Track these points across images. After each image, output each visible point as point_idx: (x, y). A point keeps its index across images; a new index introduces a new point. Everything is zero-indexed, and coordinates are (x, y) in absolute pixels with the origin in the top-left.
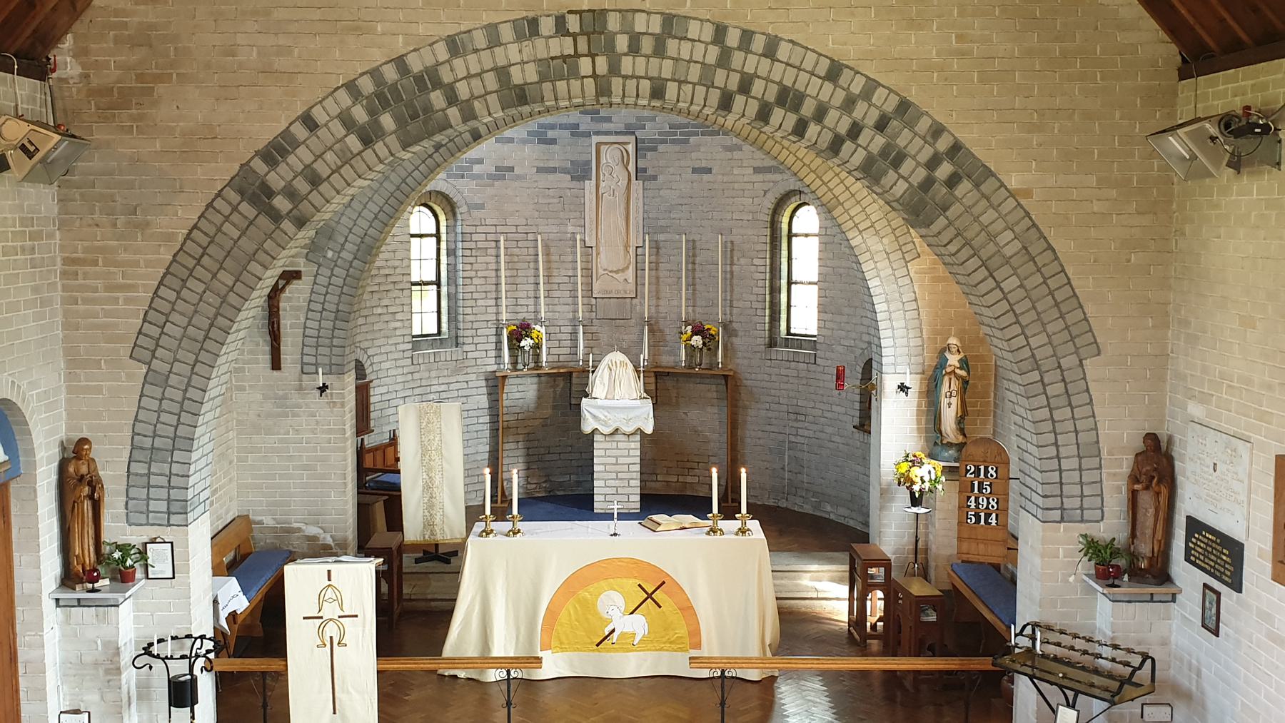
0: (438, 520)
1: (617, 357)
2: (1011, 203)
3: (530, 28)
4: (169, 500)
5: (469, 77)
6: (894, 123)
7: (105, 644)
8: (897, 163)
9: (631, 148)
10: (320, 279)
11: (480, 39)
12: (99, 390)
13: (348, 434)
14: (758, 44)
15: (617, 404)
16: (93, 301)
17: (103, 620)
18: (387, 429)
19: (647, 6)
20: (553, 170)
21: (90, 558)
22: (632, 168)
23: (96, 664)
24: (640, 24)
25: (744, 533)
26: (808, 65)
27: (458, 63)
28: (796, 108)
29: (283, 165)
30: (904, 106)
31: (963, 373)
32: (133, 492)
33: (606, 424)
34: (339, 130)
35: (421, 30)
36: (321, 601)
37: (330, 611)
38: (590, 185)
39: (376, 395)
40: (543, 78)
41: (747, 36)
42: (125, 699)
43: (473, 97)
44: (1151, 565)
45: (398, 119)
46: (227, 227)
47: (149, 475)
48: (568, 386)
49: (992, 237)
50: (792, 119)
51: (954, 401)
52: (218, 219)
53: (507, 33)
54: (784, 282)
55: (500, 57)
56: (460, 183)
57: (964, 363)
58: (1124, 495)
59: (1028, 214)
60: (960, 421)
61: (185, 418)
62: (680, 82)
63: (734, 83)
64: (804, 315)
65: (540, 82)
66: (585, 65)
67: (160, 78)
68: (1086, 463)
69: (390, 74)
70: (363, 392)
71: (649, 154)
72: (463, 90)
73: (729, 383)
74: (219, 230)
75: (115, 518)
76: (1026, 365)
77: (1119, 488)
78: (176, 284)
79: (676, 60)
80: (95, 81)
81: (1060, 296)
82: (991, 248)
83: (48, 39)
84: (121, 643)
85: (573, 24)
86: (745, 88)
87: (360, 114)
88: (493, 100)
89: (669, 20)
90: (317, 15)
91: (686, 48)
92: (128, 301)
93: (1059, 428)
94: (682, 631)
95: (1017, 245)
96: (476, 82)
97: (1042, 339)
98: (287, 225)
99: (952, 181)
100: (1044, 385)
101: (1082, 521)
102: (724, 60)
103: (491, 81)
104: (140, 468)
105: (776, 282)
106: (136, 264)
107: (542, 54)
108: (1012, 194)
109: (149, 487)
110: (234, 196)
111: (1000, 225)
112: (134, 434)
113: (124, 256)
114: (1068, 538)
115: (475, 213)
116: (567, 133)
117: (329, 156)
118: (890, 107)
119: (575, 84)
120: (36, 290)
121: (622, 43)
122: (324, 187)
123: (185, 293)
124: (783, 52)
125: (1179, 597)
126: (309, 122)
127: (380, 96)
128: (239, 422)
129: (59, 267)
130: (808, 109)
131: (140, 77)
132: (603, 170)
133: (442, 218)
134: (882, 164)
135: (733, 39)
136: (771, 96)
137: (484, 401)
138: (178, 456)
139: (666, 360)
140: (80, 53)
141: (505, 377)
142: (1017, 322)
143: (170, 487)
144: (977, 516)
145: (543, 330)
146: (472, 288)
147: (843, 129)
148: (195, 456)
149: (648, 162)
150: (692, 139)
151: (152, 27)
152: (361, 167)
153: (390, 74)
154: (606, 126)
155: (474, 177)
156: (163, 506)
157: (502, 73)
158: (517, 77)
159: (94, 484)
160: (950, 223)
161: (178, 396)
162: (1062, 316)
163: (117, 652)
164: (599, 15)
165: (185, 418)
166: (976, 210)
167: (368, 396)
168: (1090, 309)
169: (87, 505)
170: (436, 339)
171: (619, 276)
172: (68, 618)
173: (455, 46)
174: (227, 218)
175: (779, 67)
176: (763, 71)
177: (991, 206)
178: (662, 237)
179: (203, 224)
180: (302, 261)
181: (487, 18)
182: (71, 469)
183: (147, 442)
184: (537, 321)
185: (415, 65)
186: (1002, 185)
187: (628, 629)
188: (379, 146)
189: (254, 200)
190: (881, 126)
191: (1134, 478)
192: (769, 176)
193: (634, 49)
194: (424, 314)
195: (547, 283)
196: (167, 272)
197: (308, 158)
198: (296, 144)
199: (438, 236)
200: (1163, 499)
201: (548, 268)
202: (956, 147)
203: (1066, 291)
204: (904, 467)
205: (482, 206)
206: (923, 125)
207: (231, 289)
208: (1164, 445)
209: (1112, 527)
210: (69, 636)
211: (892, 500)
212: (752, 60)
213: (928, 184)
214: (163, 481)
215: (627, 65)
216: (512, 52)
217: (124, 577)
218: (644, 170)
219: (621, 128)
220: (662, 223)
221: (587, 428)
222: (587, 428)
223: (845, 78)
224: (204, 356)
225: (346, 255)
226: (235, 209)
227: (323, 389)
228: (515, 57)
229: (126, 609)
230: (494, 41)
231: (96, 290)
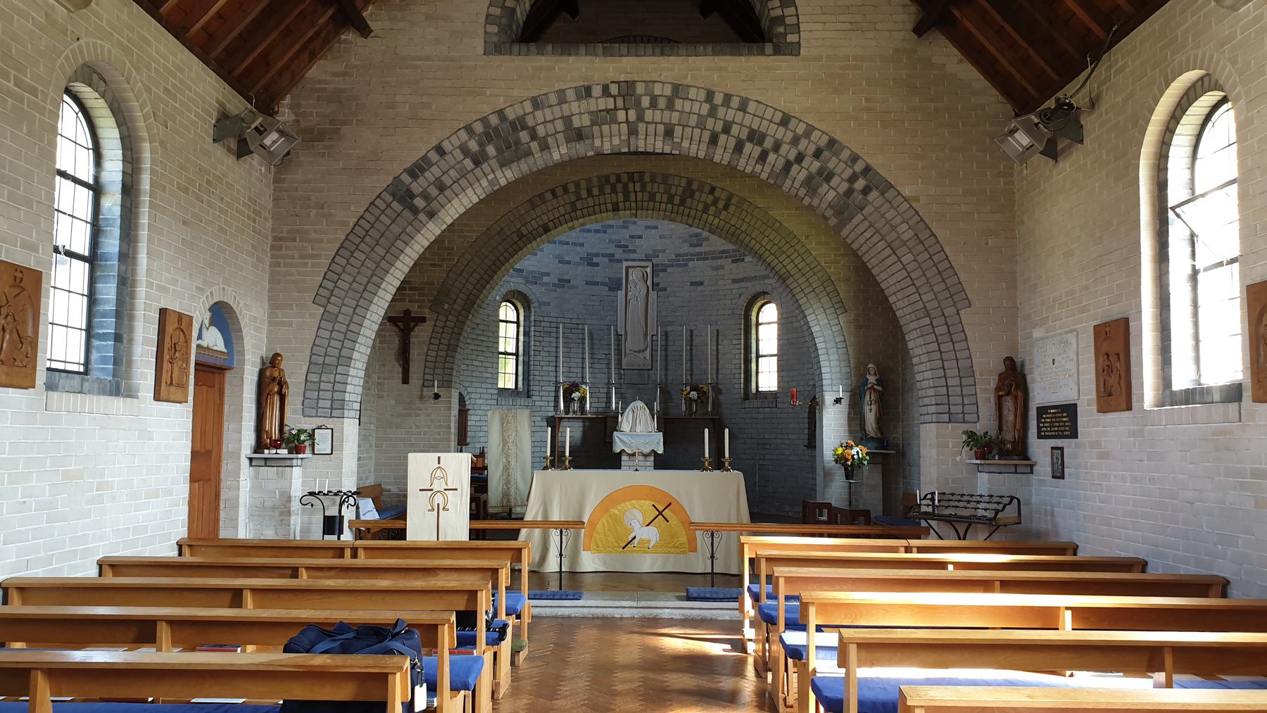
0: (513, 491)
1: (639, 404)
2: (906, 205)
4: (332, 400)
6: (826, 153)
7: (282, 494)
8: (828, 178)
9: (649, 270)
10: (440, 324)
11: (553, 99)
12: (290, 324)
14: (735, 102)
17: (281, 476)
18: (478, 446)
19: (662, 79)
20: (597, 283)
21: (275, 434)
22: (649, 283)
23: (274, 508)
24: (657, 90)
26: (768, 115)
27: (538, 114)
28: (760, 143)
29: (421, 178)
30: (832, 142)
31: (879, 388)
32: (308, 394)
33: (630, 446)
34: (458, 154)
35: (515, 93)
36: (432, 479)
37: (438, 486)
38: (621, 294)
39: (472, 420)
40: (593, 123)
41: (728, 98)
44: (1014, 448)
45: (497, 149)
46: (383, 218)
47: (319, 383)
49: (894, 228)
50: (758, 150)
51: (873, 407)
52: (377, 212)
53: (571, 95)
54: (754, 355)
57: (879, 382)
60: (879, 420)
61: (347, 343)
62: (684, 126)
63: (719, 126)
64: (768, 378)
66: (621, 115)
67: (345, 123)
68: (965, 381)
69: (494, 120)
70: (463, 413)
71: (661, 274)
72: (541, 131)
74: (377, 219)
75: (295, 412)
77: (989, 399)
78: (347, 254)
79: (681, 112)
80: (303, 124)
81: (941, 267)
82: (894, 235)
84: (293, 494)
85: (614, 89)
86: (727, 129)
87: (473, 146)
88: (560, 137)
89: (676, 88)
92: (314, 265)
95: (911, 233)
96: (550, 126)
97: (931, 296)
98: (422, 216)
99: (866, 191)
102: (713, 112)
103: (560, 125)
105: (748, 355)
107: (593, 108)
108: (906, 200)
109: (319, 390)
110: (389, 198)
111: (899, 219)
112: (312, 354)
113: (314, 236)
114: (956, 433)
115: (543, 308)
116: (606, 260)
117: (452, 172)
118: (824, 141)
119: (615, 127)
120: (254, 247)
121: (646, 101)
122: (448, 192)
123: (352, 260)
124: (752, 107)
125: (1035, 468)
126: (440, 150)
127: (487, 134)
128: (378, 420)
129: (269, 242)
130: (768, 143)
132: (630, 284)
133: (521, 311)
134: (819, 179)
135: (718, 99)
136: (744, 136)
138: (340, 369)
140: (293, 107)
141: (561, 419)
143: (334, 391)
146: (539, 358)
147: (792, 156)
149: (662, 279)
150: (690, 264)
152: (472, 179)
153: (494, 120)
154: (632, 256)
156: (328, 404)
157: (567, 120)
158: (576, 122)
159: (282, 384)
160: (865, 218)
161: (343, 328)
162: (943, 281)
163: (289, 499)
164: (631, 85)
165: (347, 343)
166: (883, 210)
167: (466, 420)
168: (962, 276)
169: (277, 398)
170: (514, 393)
172: (257, 474)
173: (537, 103)
174: (383, 212)
176: (738, 120)
179: (367, 216)
180: (427, 311)
182: (268, 373)
183: (321, 360)
184: (585, 383)
185: (511, 115)
186: (899, 193)
187: (645, 537)
188: (485, 166)
189: (401, 201)
190: (817, 154)
191: (998, 389)
192: (743, 284)
193: (653, 105)
195: (591, 358)
196: (342, 246)
198: (430, 164)
199: (518, 323)
200: (1020, 400)
201: (592, 349)
202: (867, 169)
204: (840, 451)
205: (548, 304)
206: (845, 155)
207: (383, 258)
208: (1018, 364)
209: (985, 423)
210: (256, 487)
211: (832, 481)
213: (849, 192)
214: (329, 386)
215: (648, 115)
217: (297, 449)
218: (658, 284)
219: (643, 257)
221: (617, 449)
222: (617, 449)
224: (362, 302)
226: (389, 206)
228: (576, 110)
229: (297, 472)
231: (293, 258)
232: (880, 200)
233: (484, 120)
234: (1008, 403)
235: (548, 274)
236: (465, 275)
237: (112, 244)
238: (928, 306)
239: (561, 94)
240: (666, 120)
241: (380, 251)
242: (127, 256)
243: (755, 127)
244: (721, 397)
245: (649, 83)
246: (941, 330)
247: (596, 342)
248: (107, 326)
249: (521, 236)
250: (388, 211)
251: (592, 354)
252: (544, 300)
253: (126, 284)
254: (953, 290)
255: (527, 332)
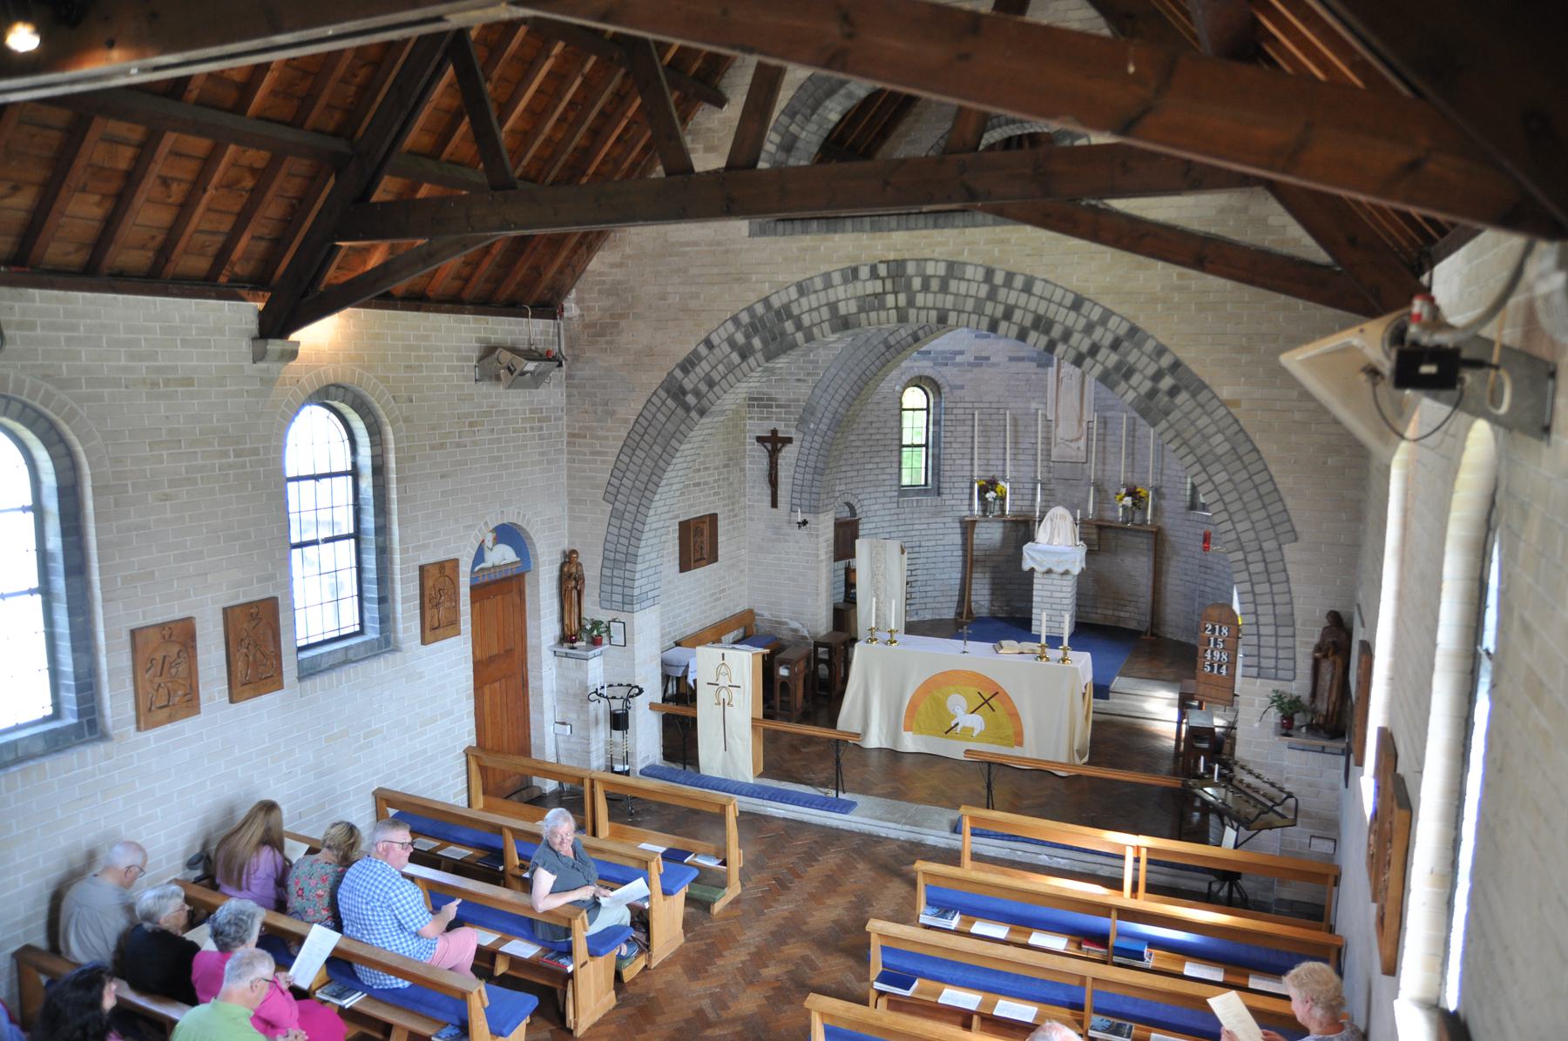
2: (1222, 411)
3: (852, 274)
5: (811, 310)
6: (1126, 344)
8: (1128, 375)
10: (806, 444)
13: (823, 557)
14: (1019, 282)
15: (1057, 548)
16: (584, 462)
19: (936, 255)
21: (575, 627)
23: (575, 695)
24: (930, 269)
25: (1064, 660)
26: (1058, 296)
27: (804, 300)
28: (1047, 331)
30: (1133, 331)
33: (1041, 565)
34: (726, 348)
35: (781, 278)
37: (723, 681)
38: (1052, 371)
40: (861, 310)
41: (1010, 276)
42: (592, 719)
43: (813, 325)
45: (764, 342)
46: (659, 415)
48: (1023, 529)
49: (1206, 438)
50: (1044, 340)
52: (654, 409)
53: (837, 278)
55: (832, 295)
56: (944, 370)
58: (1310, 662)
59: (1236, 421)
61: (633, 541)
63: (1000, 310)
65: (859, 312)
66: (890, 300)
67: (623, 316)
73: (1157, 538)
76: (1232, 546)
78: (629, 452)
79: (956, 295)
80: (587, 319)
81: (1263, 490)
82: (1205, 448)
83: (559, 293)
86: (1008, 315)
87: (740, 338)
88: (826, 326)
90: (715, 270)
91: (963, 287)
92: (603, 462)
93: (1259, 599)
94: (1010, 732)
95: (1227, 446)
96: (815, 314)
98: (694, 414)
99: (1173, 392)
100: (1247, 563)
101: (1276, 679)
102: (992, 295)
104: (607, 572)
106: (606, 438)
107: (860, 292)
108: (1223, 404)
110: (663, 394)
111: (1212, 429)
113: (600, 433)
117: (720, 367)
118: (1123, 330)
119: (883, 314)
120: (542, 454)
121: (917, 283)
122: (716, 389)
124: (1038, 288)
126: (708, 343)
127: (752, 325)
130: (1056, 332)
131: (612, 316)
134: (1116, 377)
135: (999, 279)
136: (1028, 322)
137: (958, 539)
139: (1109, 515)
140: (579, 301)
141: (974, 522)
142: (1226, 510)
144: (1212, 665)
145: (1008, 486)
147: (1084, 348)
148: (639, 567)
151: (619, 283)
152: (740, 375)
155: (955, 365)
157: (833, 307)
160: (1171, 426)
162: (1264, 507)
164: (901, 264)
165: (633, 541)
166: (1192, 416)
169: (574, 593)
170: (914, 490)
171: (1074, 445)
173: (802, 289)
175: (1034, 300)
176: (1022, 303)
177: (1206, 413)
178: (1109, 414)
179: (646, 413)
180: (793, 430)
181: (824, 268)
184: (1004, 479)
185: (776, 302)
186: (1215, 396)
187: (969, 724)
188: (751, 360)
190: (1115, 345)
191: (1318, 648)
193: (926, 287)
194: (914, 468)
197: (707, 368)
198: (700, 359)
199: (928, 409)
203: (1269, 486)
205: (962, 387)
206: (1149, 346)
209: (1299, 687)
212: (1013, 294)
213: (1152, 393)
215: (920, 299)
216: (840, 292)
217: (596, 642)
220: (1110, 402)
221: (1026, 566)
223: (1085, 309)
224: (644, 501)
225: (823, 427)
226: (664, 403)
227: (805, 523)
228: (842, 295)
230: (828, 285)
232: (1190, 404)
233: (750, 309)
234: (1326, 668)
235: (961, 353)
236: (830, 390)
237: (369, 521)
238: (1244, 537)
239: (827, 276)
240: (939, 305)
241: (657, 449)
242: (382, 530)
243: (1041, 311)
244: (1164, 503)
245: (922, 261)
246: (1257, 567)
247: (1021, 428)
248: (372, 592)
249: (889, 347)
250: (664, 409)
251: (1016, 443)
252: (958, 383)
253: (383, 552)
254: (1276, 520)
255: (937, 420)
